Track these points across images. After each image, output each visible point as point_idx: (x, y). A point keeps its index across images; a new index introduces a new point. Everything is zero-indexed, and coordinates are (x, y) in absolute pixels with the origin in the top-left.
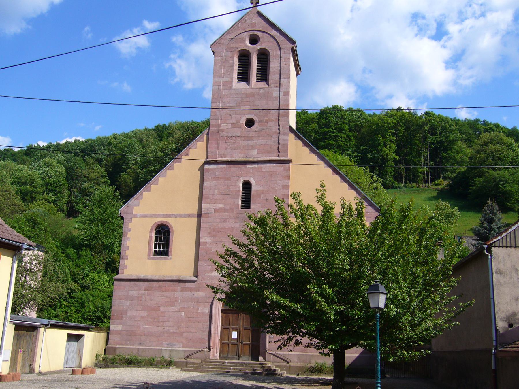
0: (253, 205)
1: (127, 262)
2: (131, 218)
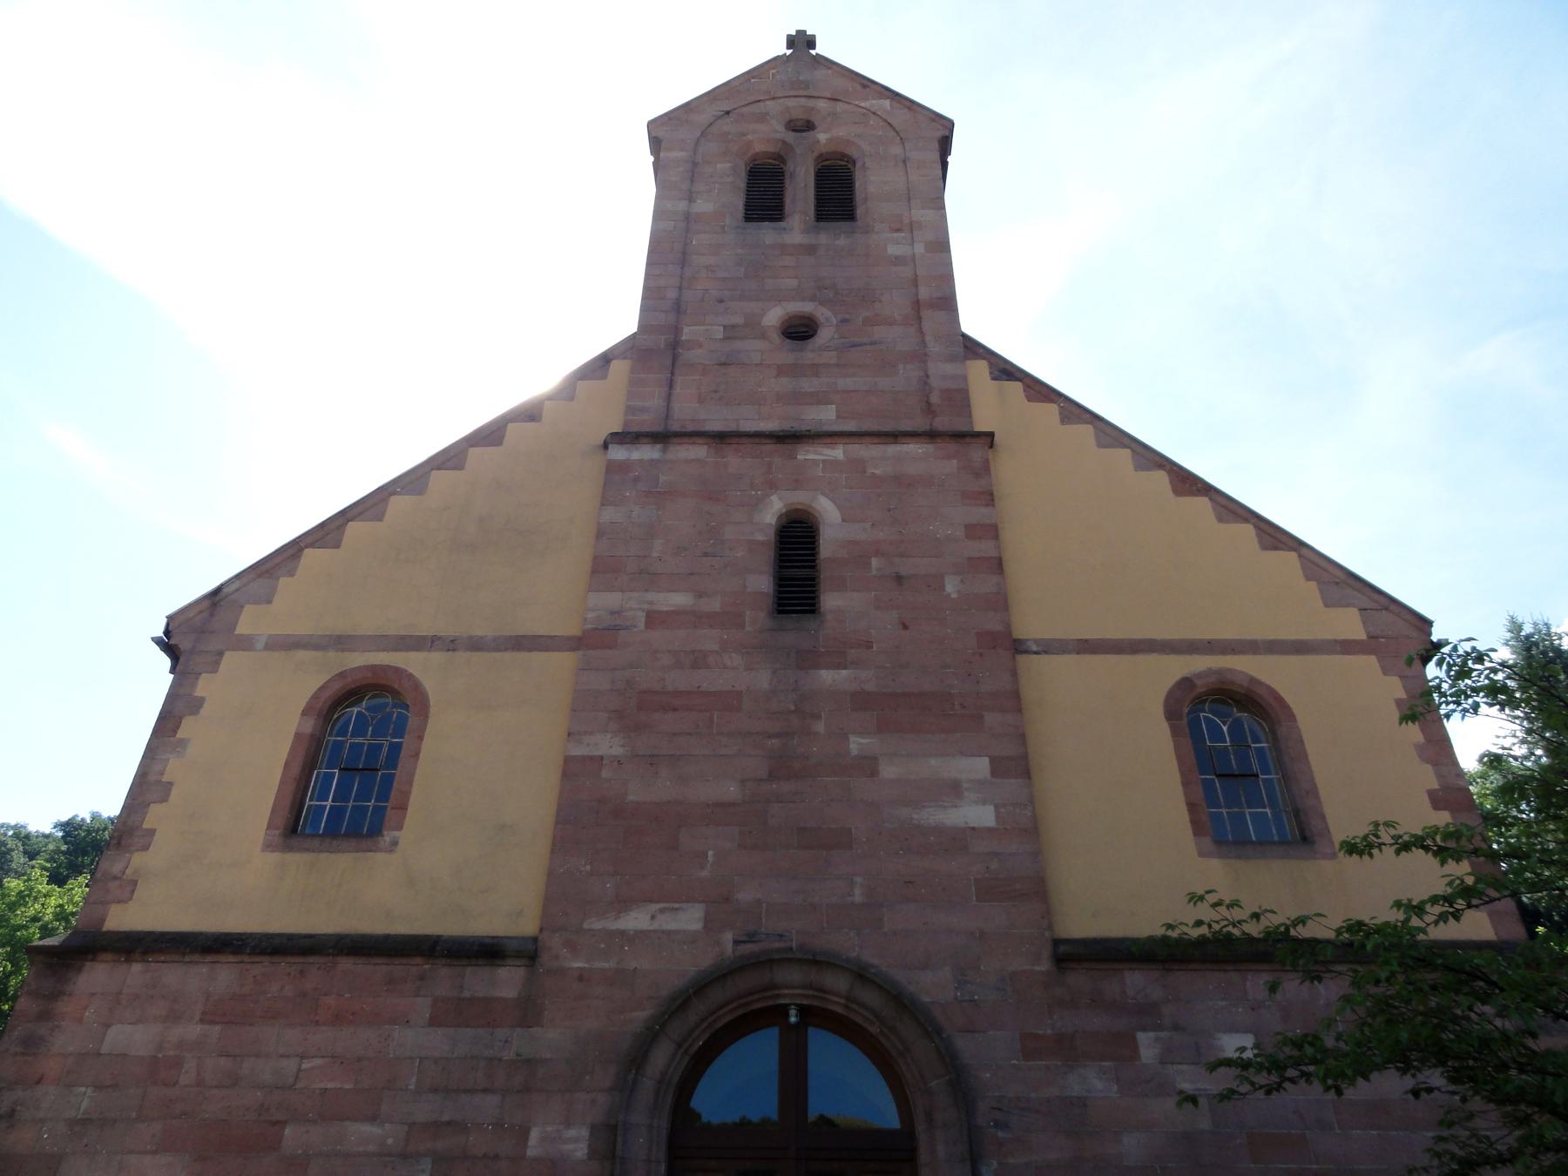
0: (830, 601)
2: (221, 654)
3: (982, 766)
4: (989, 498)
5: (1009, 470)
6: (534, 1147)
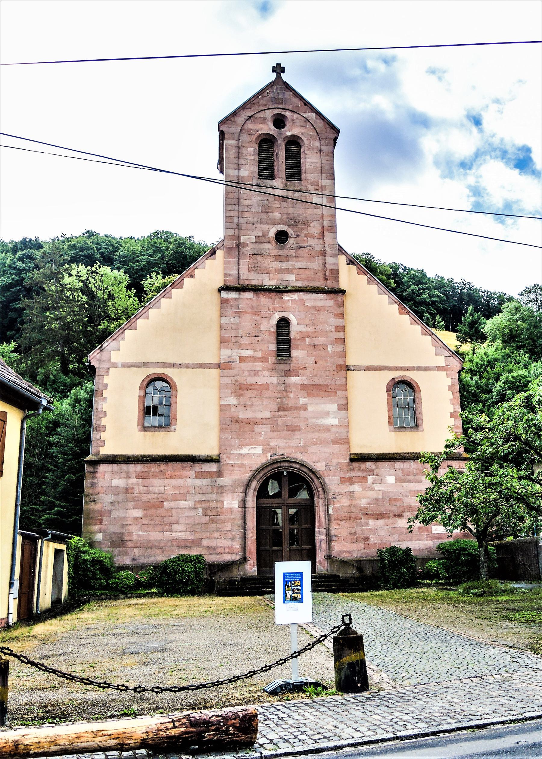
1: (104, 436)
2: (108, 369)
3: (335, 407)
4: (342, 316)
5: (350, 303)
6: (226, 505)
